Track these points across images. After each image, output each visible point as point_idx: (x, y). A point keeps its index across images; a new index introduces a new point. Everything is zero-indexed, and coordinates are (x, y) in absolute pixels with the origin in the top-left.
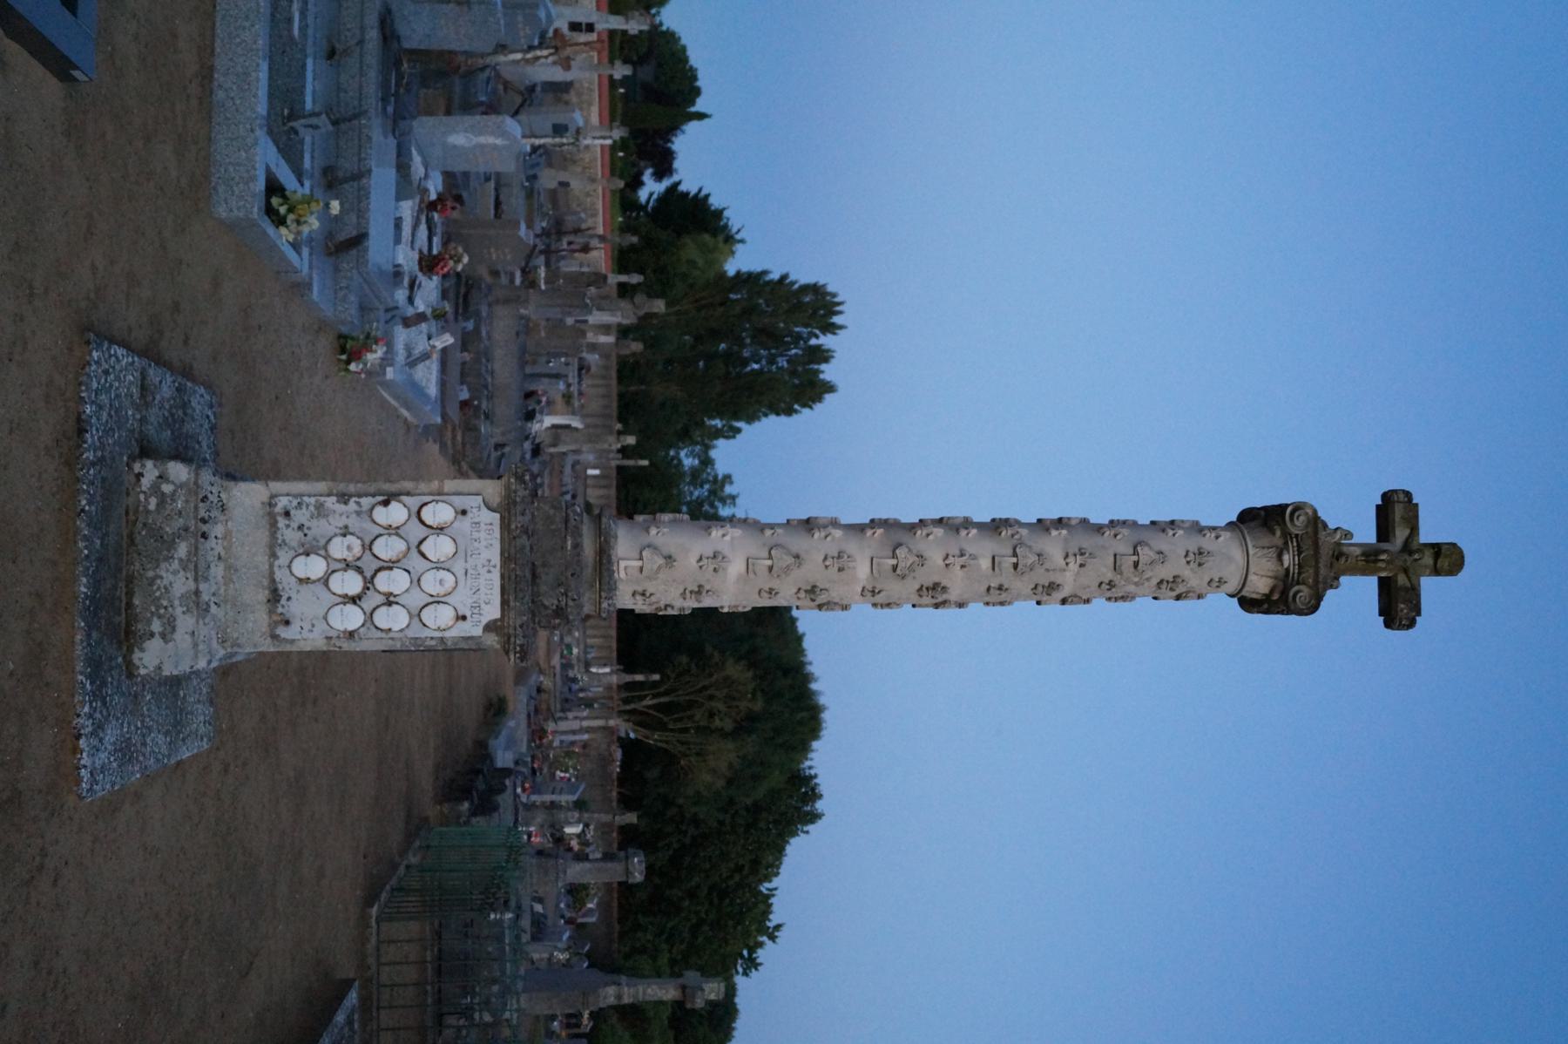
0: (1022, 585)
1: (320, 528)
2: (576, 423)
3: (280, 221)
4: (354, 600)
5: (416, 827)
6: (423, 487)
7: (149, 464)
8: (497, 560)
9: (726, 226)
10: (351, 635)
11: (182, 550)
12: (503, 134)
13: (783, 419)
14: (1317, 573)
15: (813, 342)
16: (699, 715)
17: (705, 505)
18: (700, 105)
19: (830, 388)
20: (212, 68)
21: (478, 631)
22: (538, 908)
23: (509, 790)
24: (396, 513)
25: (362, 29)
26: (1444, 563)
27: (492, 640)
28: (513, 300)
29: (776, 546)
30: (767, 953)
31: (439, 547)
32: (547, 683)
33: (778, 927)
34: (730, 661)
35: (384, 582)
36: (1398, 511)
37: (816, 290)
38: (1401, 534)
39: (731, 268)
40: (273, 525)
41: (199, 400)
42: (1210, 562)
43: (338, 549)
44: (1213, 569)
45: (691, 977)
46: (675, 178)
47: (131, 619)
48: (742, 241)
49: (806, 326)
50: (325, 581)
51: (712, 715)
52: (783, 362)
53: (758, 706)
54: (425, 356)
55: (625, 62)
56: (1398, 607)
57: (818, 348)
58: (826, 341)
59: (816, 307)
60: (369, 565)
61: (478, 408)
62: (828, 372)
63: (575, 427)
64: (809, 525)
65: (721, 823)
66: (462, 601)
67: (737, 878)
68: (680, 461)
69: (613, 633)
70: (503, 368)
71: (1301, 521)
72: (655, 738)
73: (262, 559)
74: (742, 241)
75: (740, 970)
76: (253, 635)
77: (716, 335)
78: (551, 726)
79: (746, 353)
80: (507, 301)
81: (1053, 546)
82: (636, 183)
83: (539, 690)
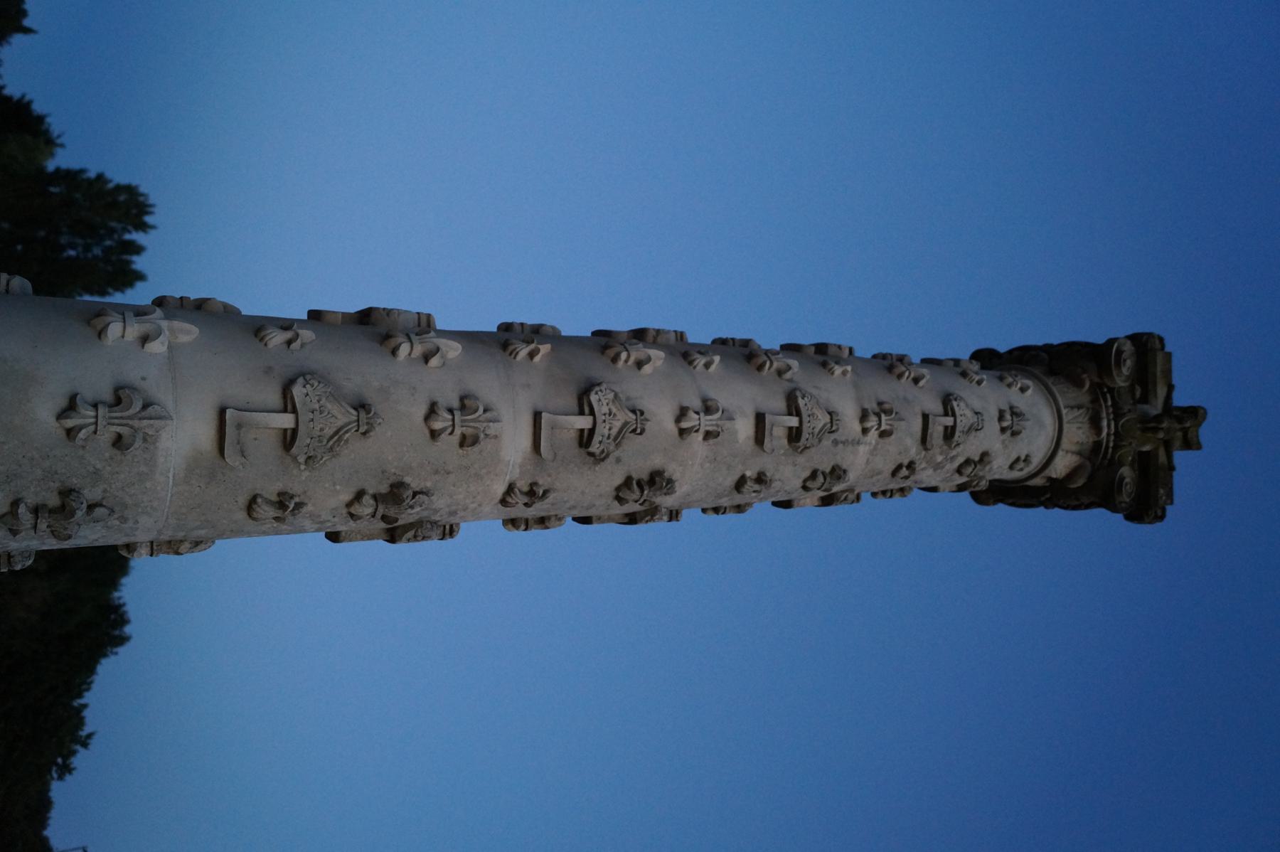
15: (127, 237)
18: (27, 22)
29: (304, 374)
30: (81, 759)
33: (90, 736)
37: (130, 190)
39: (51, 166)
48: (62, 146)
49: (119, 221)
59: (130, 207)
62: (139, 263)
64: (372, 326)
74: (62, 146)
75: (55, 775)
79: (64, 240)
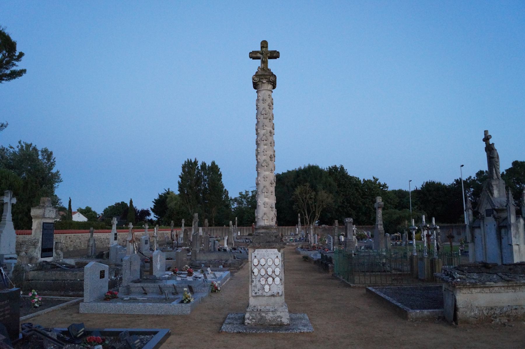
0: (270, 139)
1: (259, 286)
2: (226, 238)
3: (189, 301)
4: (274, 279)
5: (334, 277)
6: (250, 265)
7: (246, 321)
8: (265, 250)
9: (164, 194)
10: (281, 280)
11: (263, 314)
12: (157, 255)
13: (222, 177)
14: (267, 75)
15: (200, 168)
16: (310, 202)
17: (251, 202)
18: (128, 203)
19: (213, 163)
20: (157, 315)
21: (280, 254)
22: (363, 248)
23: (327, 254)
24: (256, 271)
25: (138, 287)
26: (265, 46)
27: (282, 251)
28: (195, 253)
31: (263, 262)
32: (300, 246)
33: (374, 178)
34: (295, 193)
35: (270, 273)
36: (254, 55)
37: (184, 167)
38: (259, 55)
39: (177, 192)
40: (259, 296)
41: (230, 316)
42: (265, 98)
43: (263, 282)
44: (267, 97)
45: (376, 205)
46: (150, 209)
47: (277, 324)
48: (169, 189)
49: (195, 170)
50: (270, 285)
51: (311, 198)
52: (206, 177)
53: (308, 184)
54: (214, 274)
55: (128, 224)
56: (275, 55)
57: (201, 166)
58: (199, 164)
59: (189, 167)
60: (266, 276)
61: (224, 263)
62: (209, 164)
63: (228, 238)
65: (343, 195)
66: (274, 257)
67: (360, 190)
68: (236, 208)
69: (287, 227)
70: (214, 257)
71: (256, 79)
72: (318, 215)
73: (265, 298)
74: (169, 189)
76: (281, 300)
77: (197, 197)
78: (312, 245)
79: (203, 188)
80: (196, 256)
81: (262, 132)
82: (151, 221)
83: (302, 248)
